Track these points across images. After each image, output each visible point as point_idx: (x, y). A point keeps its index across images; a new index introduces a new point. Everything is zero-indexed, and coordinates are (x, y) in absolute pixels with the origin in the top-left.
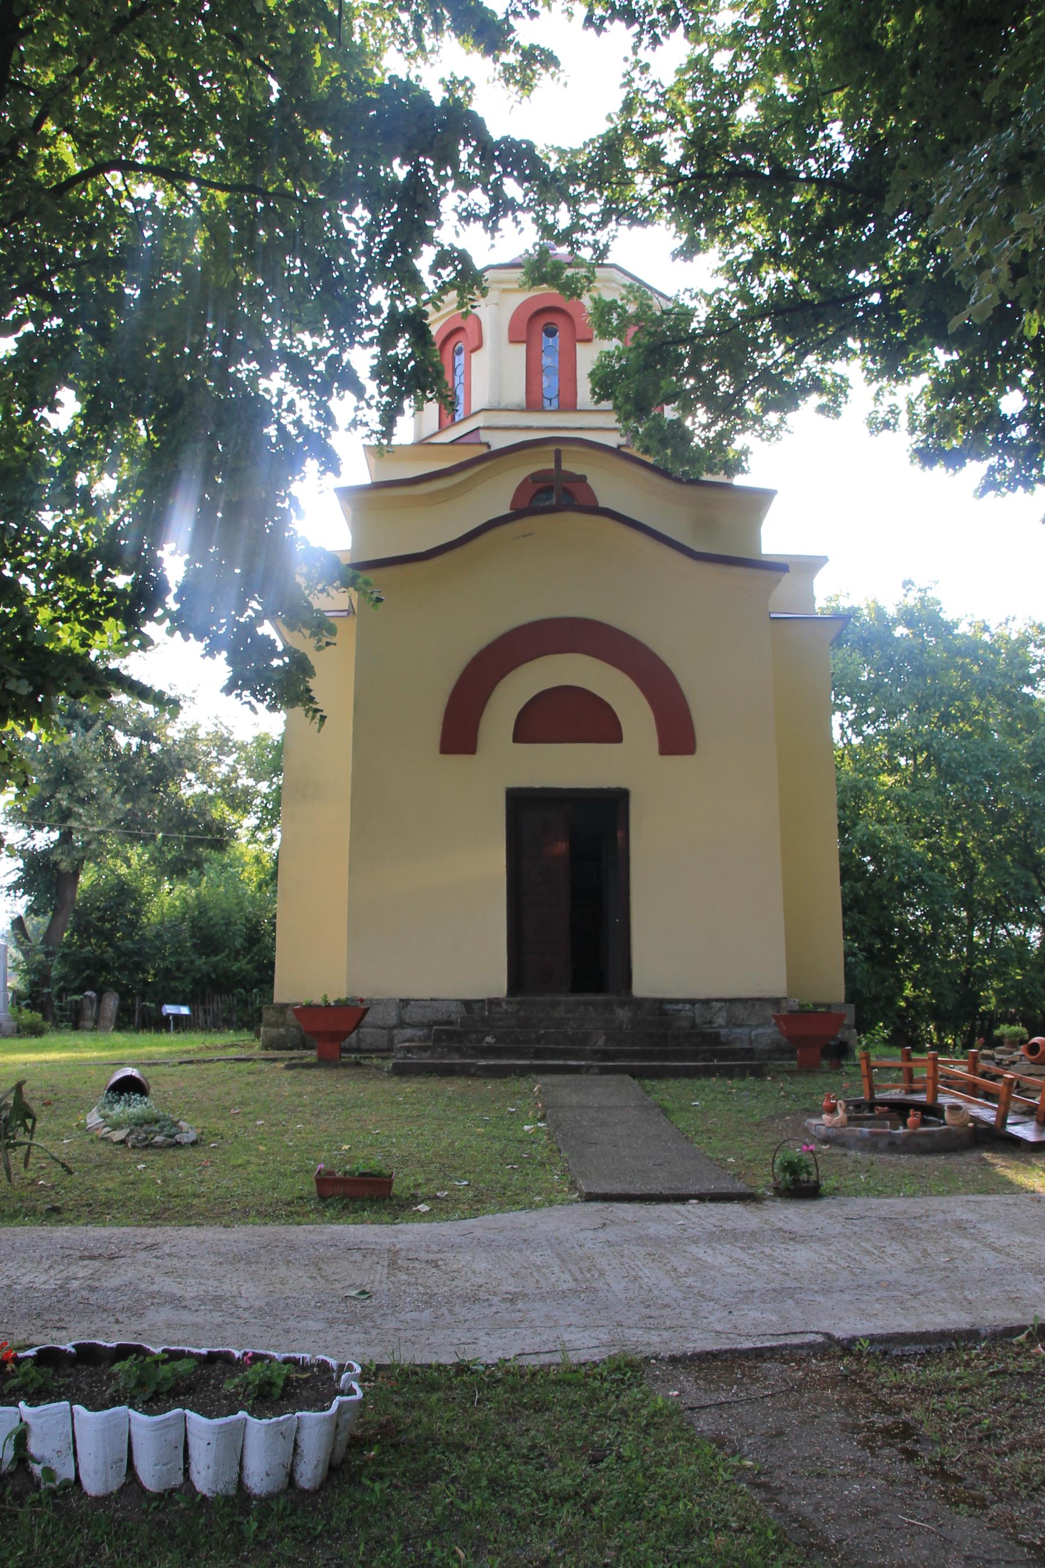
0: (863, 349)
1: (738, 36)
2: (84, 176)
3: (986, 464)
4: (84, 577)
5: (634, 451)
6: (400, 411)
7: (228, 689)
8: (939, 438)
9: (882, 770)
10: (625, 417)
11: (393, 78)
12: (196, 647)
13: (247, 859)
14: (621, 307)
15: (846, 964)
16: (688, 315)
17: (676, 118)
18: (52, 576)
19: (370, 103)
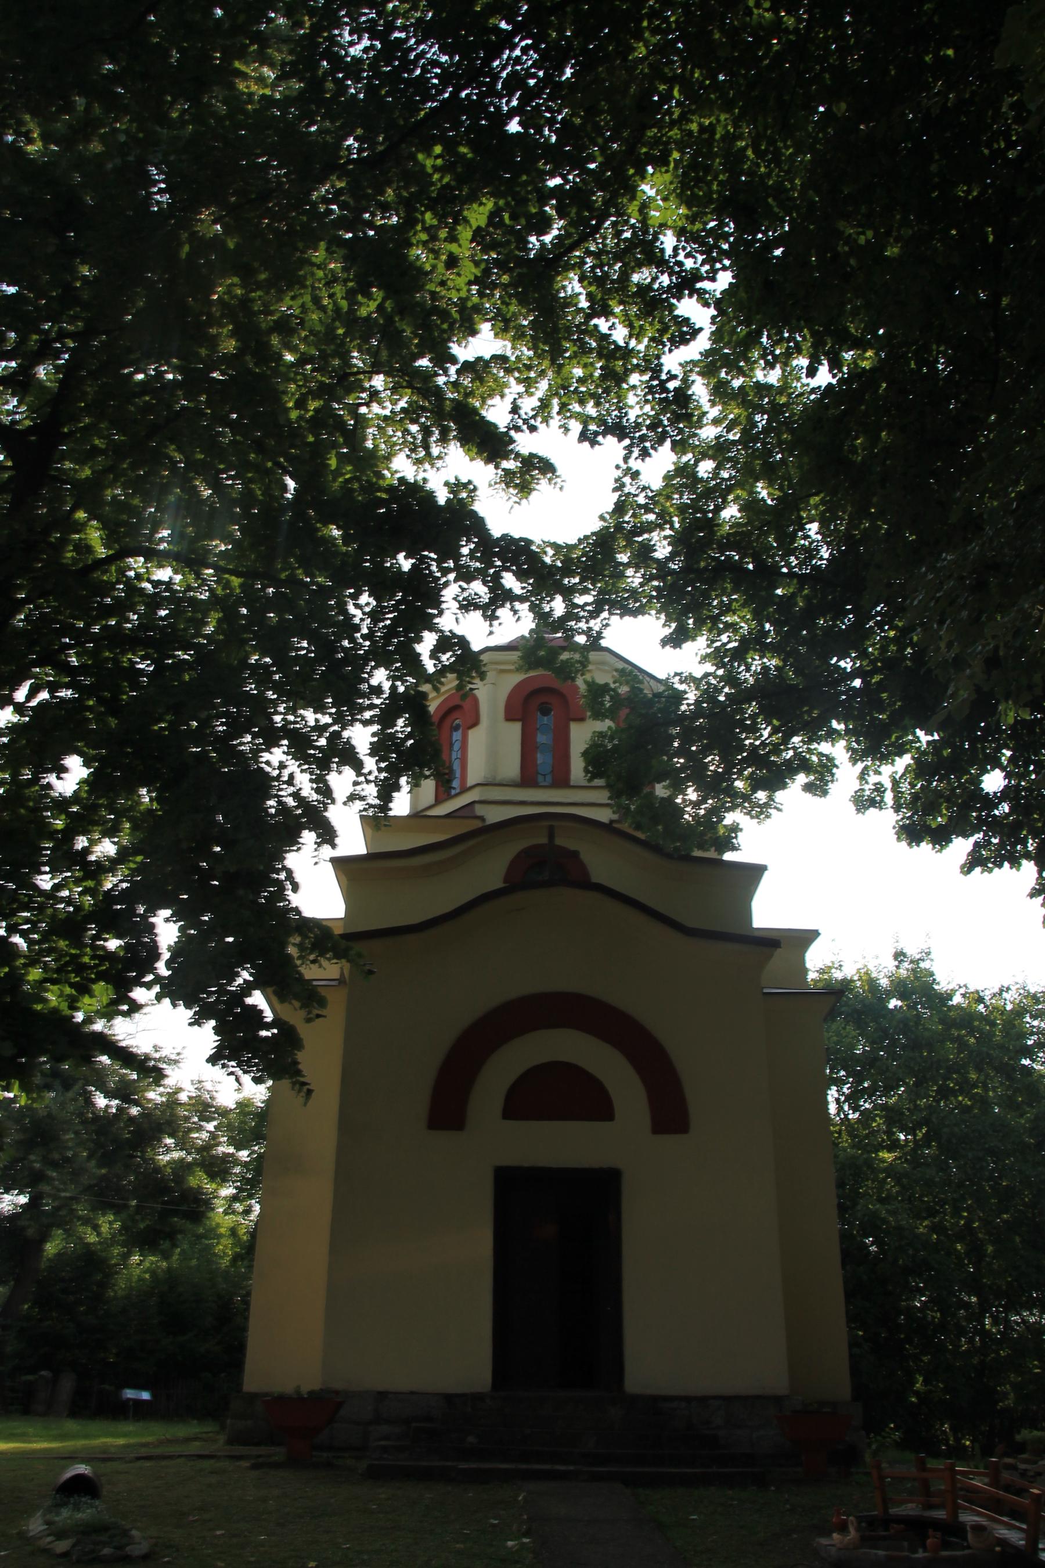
0: (847, 731)
1: (718, 450)
2: (109, 560)
3: (972, 840)
4: (76, 940)
5: (625, 827)
6: (397, 788)
7: (213, 1060)
8: (925, 814)
9: (880, 1147)
10: (616, 794)
11: (402, 480)
12: (184, 1014)
13: (222, 1230)
14: (614, 690)
15: (851, 1356)
16: (678, 697)
17: (664, 519)
18: (46, 937)
19: (382, 503)
